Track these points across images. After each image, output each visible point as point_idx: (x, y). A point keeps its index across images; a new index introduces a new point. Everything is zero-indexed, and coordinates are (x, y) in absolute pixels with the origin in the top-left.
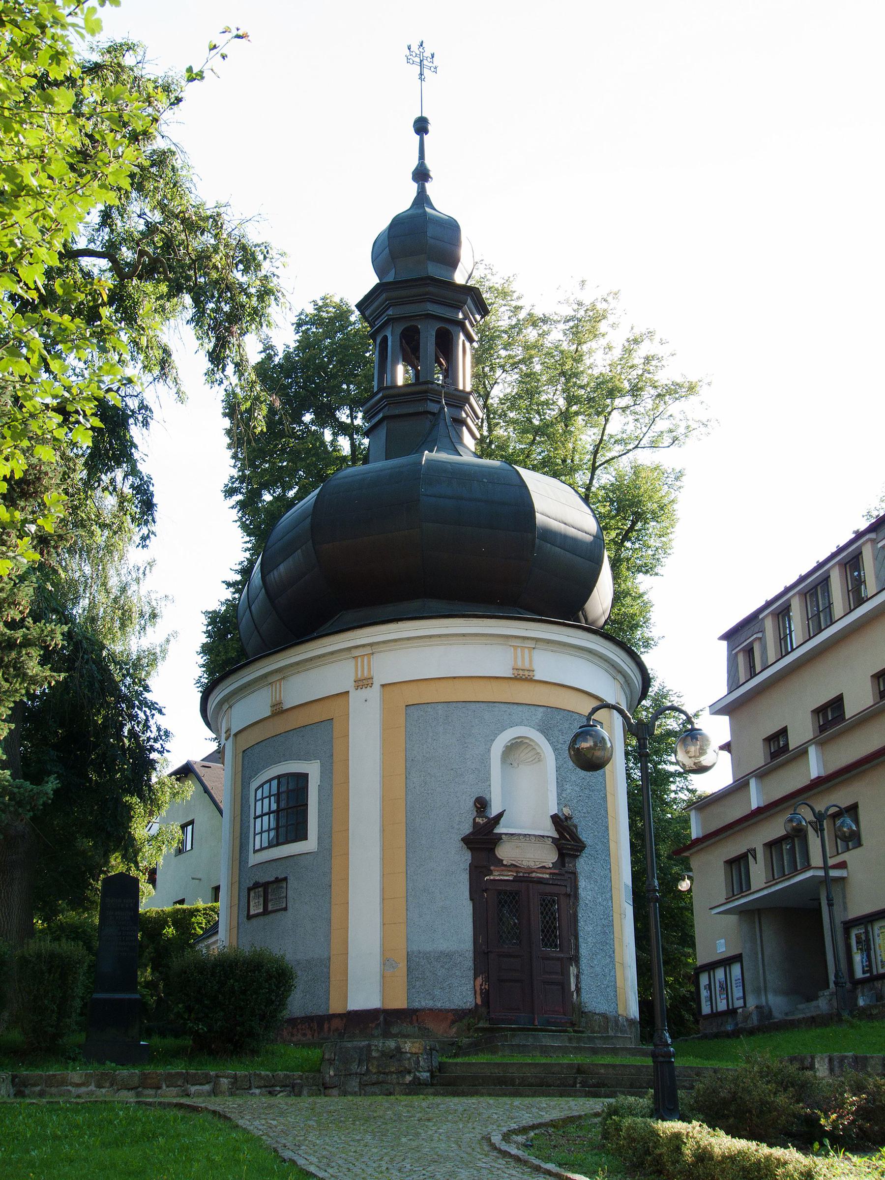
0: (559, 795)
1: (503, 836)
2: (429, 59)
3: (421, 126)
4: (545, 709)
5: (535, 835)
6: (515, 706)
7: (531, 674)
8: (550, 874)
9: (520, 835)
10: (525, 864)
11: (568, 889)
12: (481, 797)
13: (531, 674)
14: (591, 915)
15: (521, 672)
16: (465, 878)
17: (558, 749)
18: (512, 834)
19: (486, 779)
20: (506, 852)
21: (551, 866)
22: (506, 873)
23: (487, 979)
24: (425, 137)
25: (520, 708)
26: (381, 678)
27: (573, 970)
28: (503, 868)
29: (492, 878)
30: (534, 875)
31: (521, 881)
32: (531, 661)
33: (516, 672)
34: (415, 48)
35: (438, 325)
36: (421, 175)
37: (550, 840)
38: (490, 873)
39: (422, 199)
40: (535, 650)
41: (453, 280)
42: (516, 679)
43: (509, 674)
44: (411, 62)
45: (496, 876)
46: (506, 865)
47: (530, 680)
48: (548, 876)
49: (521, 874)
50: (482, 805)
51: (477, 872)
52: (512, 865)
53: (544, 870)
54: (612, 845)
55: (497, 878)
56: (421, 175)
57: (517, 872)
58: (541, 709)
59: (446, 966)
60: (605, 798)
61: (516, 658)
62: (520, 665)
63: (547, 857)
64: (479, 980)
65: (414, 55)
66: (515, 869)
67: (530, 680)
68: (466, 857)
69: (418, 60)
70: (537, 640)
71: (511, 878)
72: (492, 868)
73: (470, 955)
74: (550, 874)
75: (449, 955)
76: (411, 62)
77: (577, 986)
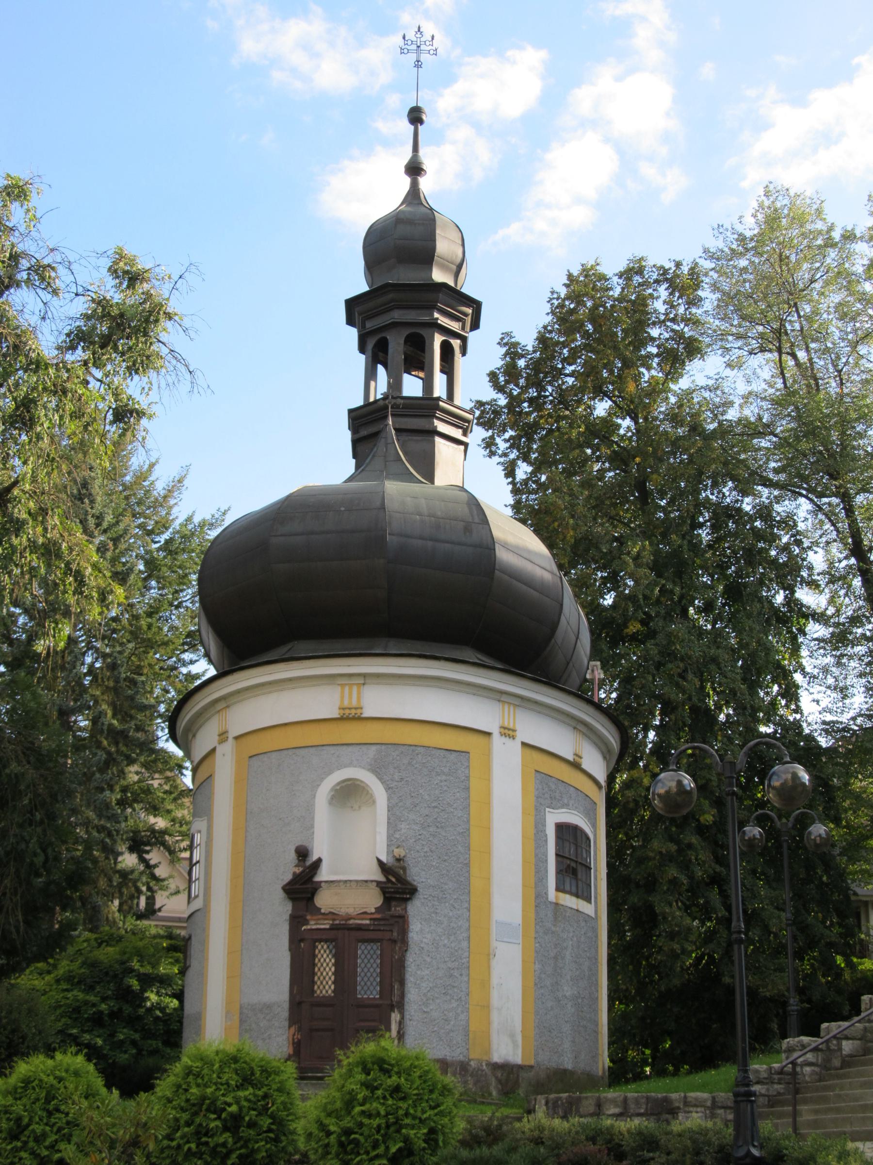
0: (390, 837)
1: (323, 884)
2: (428, 43)
3: (416, 116)
4: (378, 746)
5: (357, 881)
6: (345, 747)
7: (359, 711)
8: (371, 919)
9: (340, 881)
10: (343, 911)
11: (395, 934)
12: (301, 846)
13: (359, 711)
14: (428, 959)
15: (347, 712)
16: (285, 928)
17: (392, 788)
18: (332, 882)
19: (309, 827)
20: (324, 900)
21: (373, 910)
22: (322, 922)
23: (300, 1030)
24: (420, 128)
25: (350, 748)
26: (235, 732)
27: (395, 1017)
28: (320, 917)
29: (309, 927)
30: (351, 922)
31: (338, 929)
32: (359, 698)
33: (342, 712)
34: (411, 35)
35: (406, 332)
36: (414, 169)
37: (375, 884)
38: (306, 922)
39: (414, 195)
40: (366, 686)
41: (433, 280)
42: (342, 719)
43: (336, 716)
44: (406, 51)
45: (312, 925)
46: (324, 914)
47: (359, 719)
48: (368, 922)
49: (337, 922)
50: (302, 853)
51: (296, 921)
52: (331, 913)
53: (365, 916)
54: (476, 883)
55: (314, 927)
56: (414, 169)
57: (334, 920)
58: (374, 748)
59: (267, 1018)
60: (466, 834)
61: (342, 697)
62: (346, 703)
63: (372, 901)
64: (293, 1029)
65: (409, 43)
66: (330, 916)
67: (359, 719)
68: (287, 908)
69: (414, 47)
70: (364, 676)
71: (327, 927)
72: (308, 917)
73: (286, 1006)
74: (371, 919)
75: (269, 1006)
76: (406, 51)
77: (399, 1032)
